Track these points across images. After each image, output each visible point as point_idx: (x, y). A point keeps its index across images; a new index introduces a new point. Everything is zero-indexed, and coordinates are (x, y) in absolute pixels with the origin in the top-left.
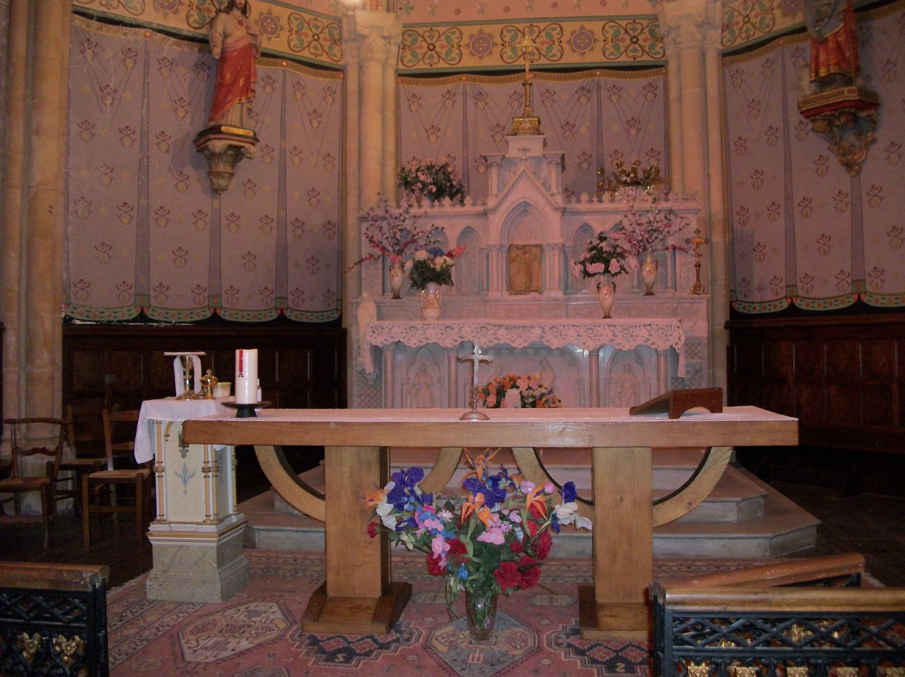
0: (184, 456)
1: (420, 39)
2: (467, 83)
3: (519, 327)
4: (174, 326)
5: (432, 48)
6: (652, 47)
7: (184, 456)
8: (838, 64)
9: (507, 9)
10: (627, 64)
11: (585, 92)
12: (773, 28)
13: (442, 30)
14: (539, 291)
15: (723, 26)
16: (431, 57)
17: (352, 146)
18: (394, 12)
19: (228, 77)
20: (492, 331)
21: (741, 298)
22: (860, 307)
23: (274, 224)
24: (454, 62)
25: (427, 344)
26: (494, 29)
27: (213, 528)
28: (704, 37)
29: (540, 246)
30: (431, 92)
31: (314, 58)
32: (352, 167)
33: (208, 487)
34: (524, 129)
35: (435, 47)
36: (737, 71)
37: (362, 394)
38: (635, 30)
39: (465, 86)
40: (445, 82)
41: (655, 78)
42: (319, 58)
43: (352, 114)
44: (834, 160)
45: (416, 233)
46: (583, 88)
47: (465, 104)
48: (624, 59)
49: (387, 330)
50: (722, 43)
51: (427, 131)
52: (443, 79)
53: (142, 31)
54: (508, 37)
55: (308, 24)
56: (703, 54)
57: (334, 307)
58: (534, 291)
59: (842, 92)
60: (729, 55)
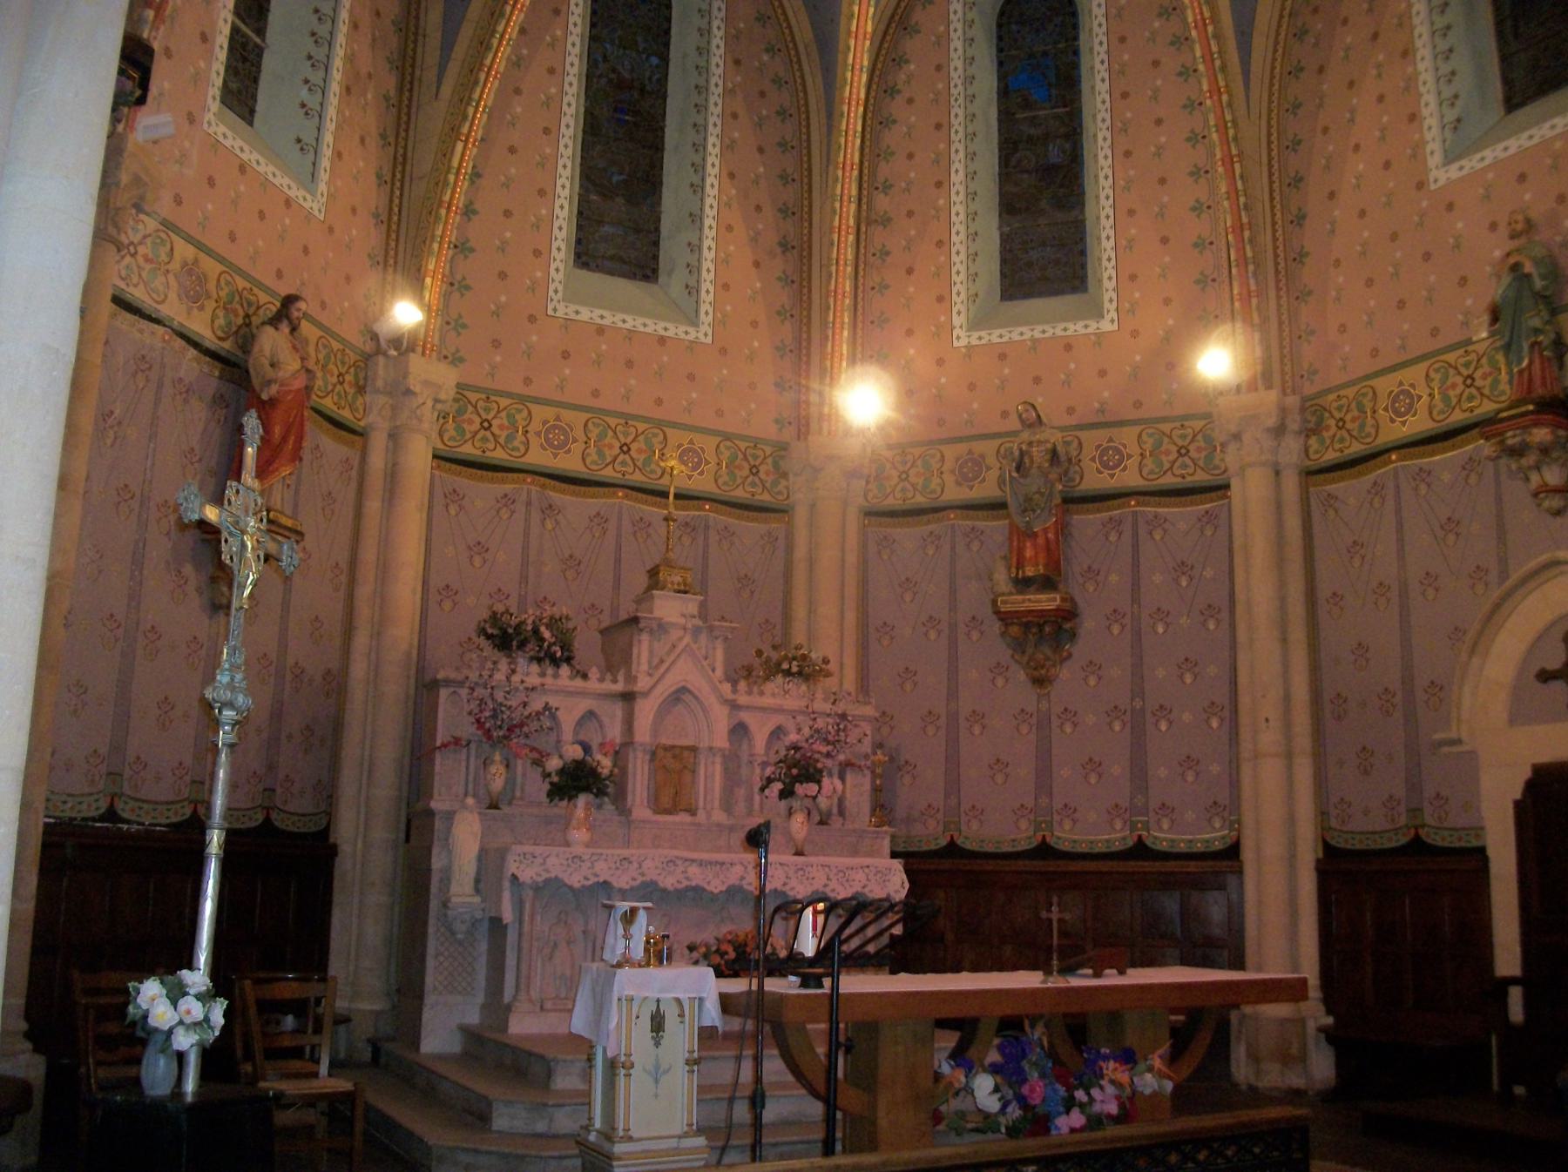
0: (657, 1044)
1: (470, 408)
2: (533, 488)
3: (717, 862)
4: (147, 831)
5: (486, 425)
6: (776, 483)
7: (657, 1044)
9: (596, 394)
10: (472, 459)
11: (689, 530)
13: (504, 402)
14: (692, 812)
16: (484, 439)
17: (369, 554)
19: (277, 431)
20: (682, 869)
22: (952, 850)
23: (1127, 717)
25: (643, 883)
26: (576, 419)
27: (701, 1141)
29: (693, 749)
30: (482, 492)
32: (364, 591)
33: (604, 1094)
34: (672, 583)
35: (490, 425)
37: (442, 954)
38: (626, 434)
39: (529, 493)
40: (503, 481)
41: (775, 526)
42: (341, 412)
43: (373, 505)
45: (526, 713)
46: (687, 524)
47: (527, 520)
48: (740, 494)
49: (540, 860)
51: (470, 548)
52: (500, 475)
53: (160, 330)
54: (594, 432)
55: (475, 407)
57: (323, 808)
58: (686, 810)
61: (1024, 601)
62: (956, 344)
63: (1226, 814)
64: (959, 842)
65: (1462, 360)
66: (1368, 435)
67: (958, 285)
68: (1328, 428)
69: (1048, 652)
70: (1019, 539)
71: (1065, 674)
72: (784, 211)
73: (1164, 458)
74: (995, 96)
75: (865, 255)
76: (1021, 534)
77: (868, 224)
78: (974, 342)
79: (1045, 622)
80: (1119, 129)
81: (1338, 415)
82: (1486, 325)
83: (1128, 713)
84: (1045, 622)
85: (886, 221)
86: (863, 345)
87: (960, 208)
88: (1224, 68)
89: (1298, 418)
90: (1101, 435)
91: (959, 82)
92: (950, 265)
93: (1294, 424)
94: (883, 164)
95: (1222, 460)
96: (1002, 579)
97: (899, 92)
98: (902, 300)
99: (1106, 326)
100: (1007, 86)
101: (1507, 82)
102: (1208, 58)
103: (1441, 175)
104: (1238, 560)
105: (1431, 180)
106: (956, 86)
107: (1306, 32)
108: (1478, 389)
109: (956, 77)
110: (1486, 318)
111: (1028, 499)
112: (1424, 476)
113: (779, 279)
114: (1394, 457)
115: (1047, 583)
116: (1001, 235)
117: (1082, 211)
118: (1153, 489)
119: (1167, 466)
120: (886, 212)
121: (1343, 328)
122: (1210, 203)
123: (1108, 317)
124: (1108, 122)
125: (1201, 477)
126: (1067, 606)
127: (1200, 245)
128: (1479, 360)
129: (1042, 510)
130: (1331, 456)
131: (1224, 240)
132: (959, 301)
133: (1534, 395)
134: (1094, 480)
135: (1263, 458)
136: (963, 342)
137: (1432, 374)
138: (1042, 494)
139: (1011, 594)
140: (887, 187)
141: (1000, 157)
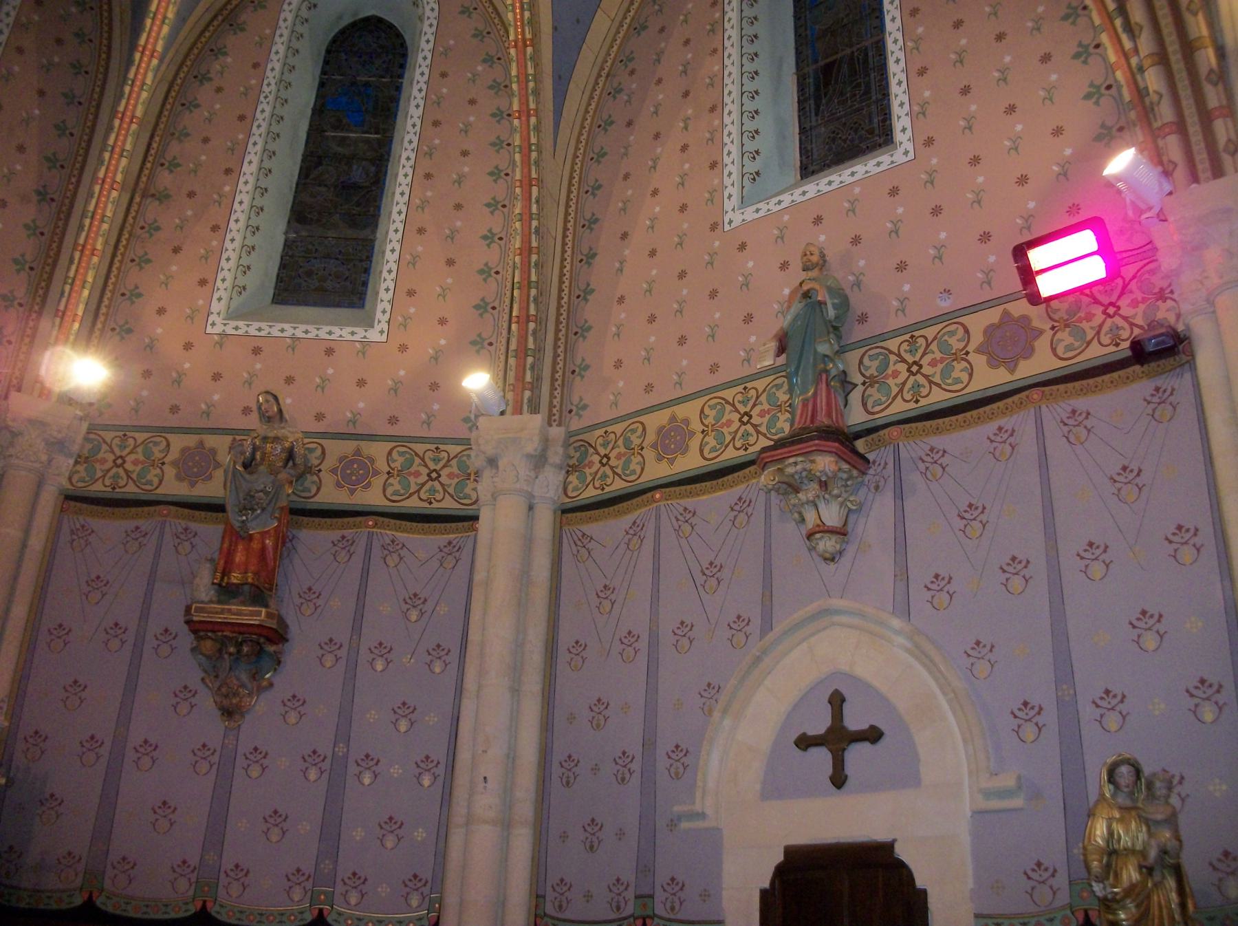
8: (256, 574)
12: (157, 488)
13: (930, 332)
15: (79, 456)
18: (559, 425)
21: (664, 914)
23: (326, 765)
24: (877, 409)
28: (50, 461)
31: (428, 506)
36: (83, 526)
44: (207, 702)
50: (70, 479)
56: (40, 484)
59: (259, 613)
60: (74, 499)
61: (223, 611)
62: (209, 330)
63: (426, 890)
64: (99, 902)
65: (739, 397)
66: (634, 472)
67: (226, 273)
68: (591, 464)
69: (244, 677)
70: (231, 542)
71: (263, 708)
72: (52, 161)
73: (412, 479)
74: (309, 112)
75: (132, 226)
76: (235, 536)
77: (143, 196)
78: (230, 331)
79: (244, 641)
80: (425, 152)
81: (602, 451)
82: (772, 353)
83: (328, 761)
84: (244, 641)
85: (163, 197)
86: (107, 315)
87: (246, 199)
88: (536, 92)
89: (561, 450)
90: (349, 447)
91: (273, 82)
92: (222, 249)
93: (556, 455)
94: (174, 143)
95: (475, 489)
96: (204, 588)
97: (210, 79)
98: (162, 277)
99: (374, 335)
100: (323, 105)
101: (804, 151)
102: (523, 78)
103: (735, 217)
104: (477, 594)
105: (727, 220)
106: (269, 85)
107: (621, 90)
108: (755, 426)
109: (272, 76)
110: (773, 346)
111: (250, 496)
112: (688, 516)
113: (27, 226)
114: (658, 496)
115: (259, 596)
116: (286, 241)
117: (374, 232)
118: (396, 511)
119: (413, 488)
120: (166, 189)
121: (618, 364)
122: (502, 235)
123: (378, 328)
124: (415, 144)
125: (448, 505)
126: (272, 624)
127: (486, 272)
128: (758, 397)
129: (263, 510)
130: (591, 493)
131: (508, 294)
132: (223, 288)
133: (817, 424)
134: (330, 494)
135: (518, 486)
136: (218, 329)
137: (707, 411)
138: (267, 493)
139: (211, 602)
140: (174, 165)
141: (301, 168)
